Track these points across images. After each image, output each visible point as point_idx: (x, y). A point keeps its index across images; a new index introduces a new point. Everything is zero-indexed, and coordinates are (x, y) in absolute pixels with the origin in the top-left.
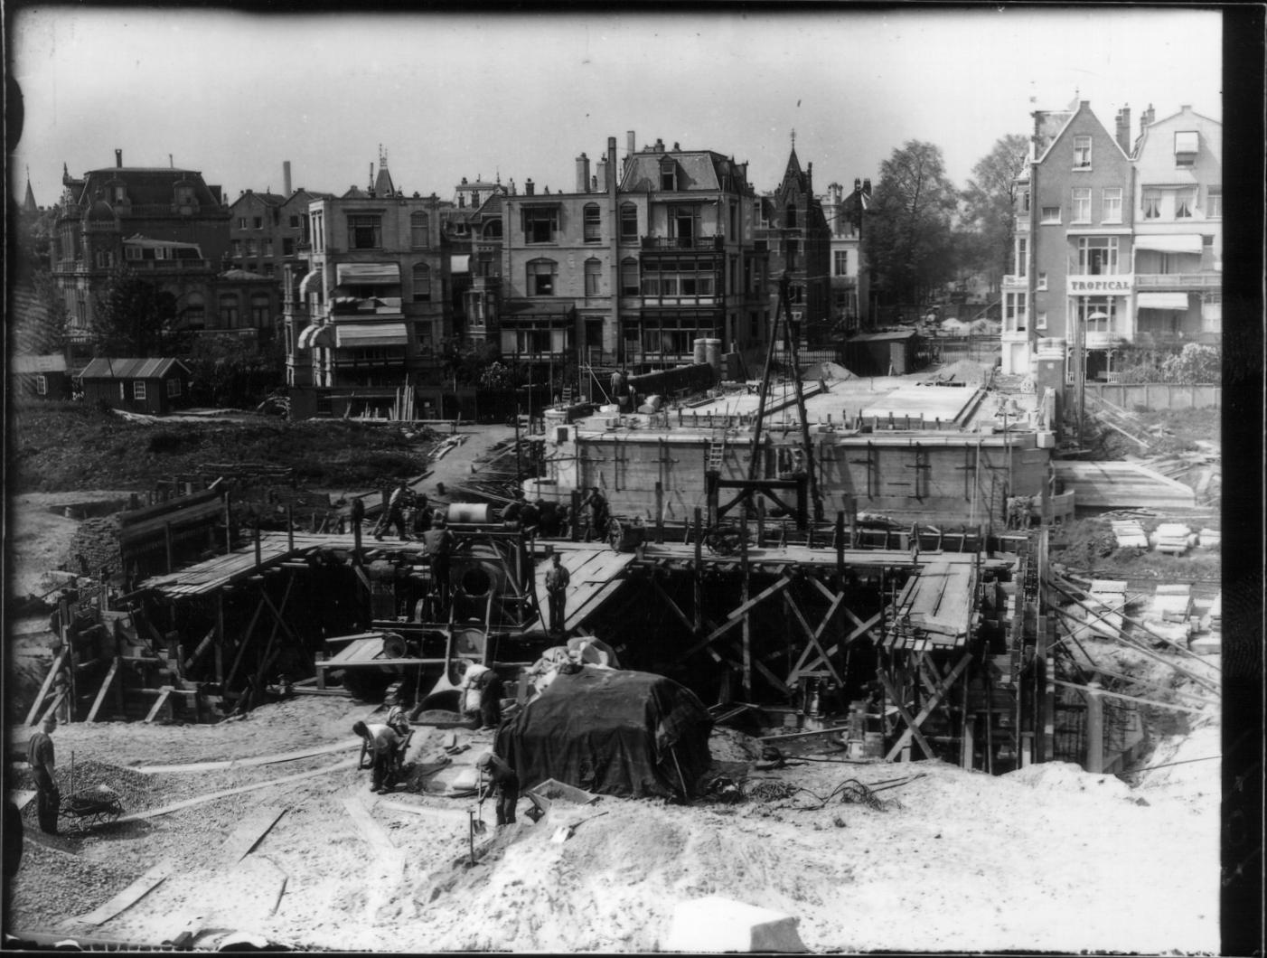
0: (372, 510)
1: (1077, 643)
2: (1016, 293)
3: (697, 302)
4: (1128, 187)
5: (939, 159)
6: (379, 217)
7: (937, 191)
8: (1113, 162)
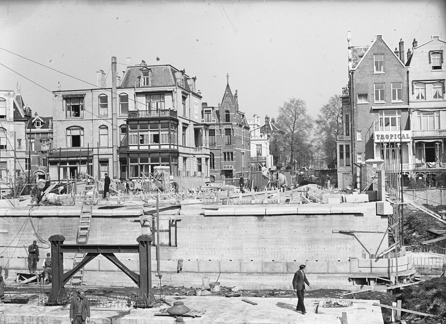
0: (80, 242)
2: (344, 144)
5: (304, 105)
7: (303, 120)
8: (396, 68)
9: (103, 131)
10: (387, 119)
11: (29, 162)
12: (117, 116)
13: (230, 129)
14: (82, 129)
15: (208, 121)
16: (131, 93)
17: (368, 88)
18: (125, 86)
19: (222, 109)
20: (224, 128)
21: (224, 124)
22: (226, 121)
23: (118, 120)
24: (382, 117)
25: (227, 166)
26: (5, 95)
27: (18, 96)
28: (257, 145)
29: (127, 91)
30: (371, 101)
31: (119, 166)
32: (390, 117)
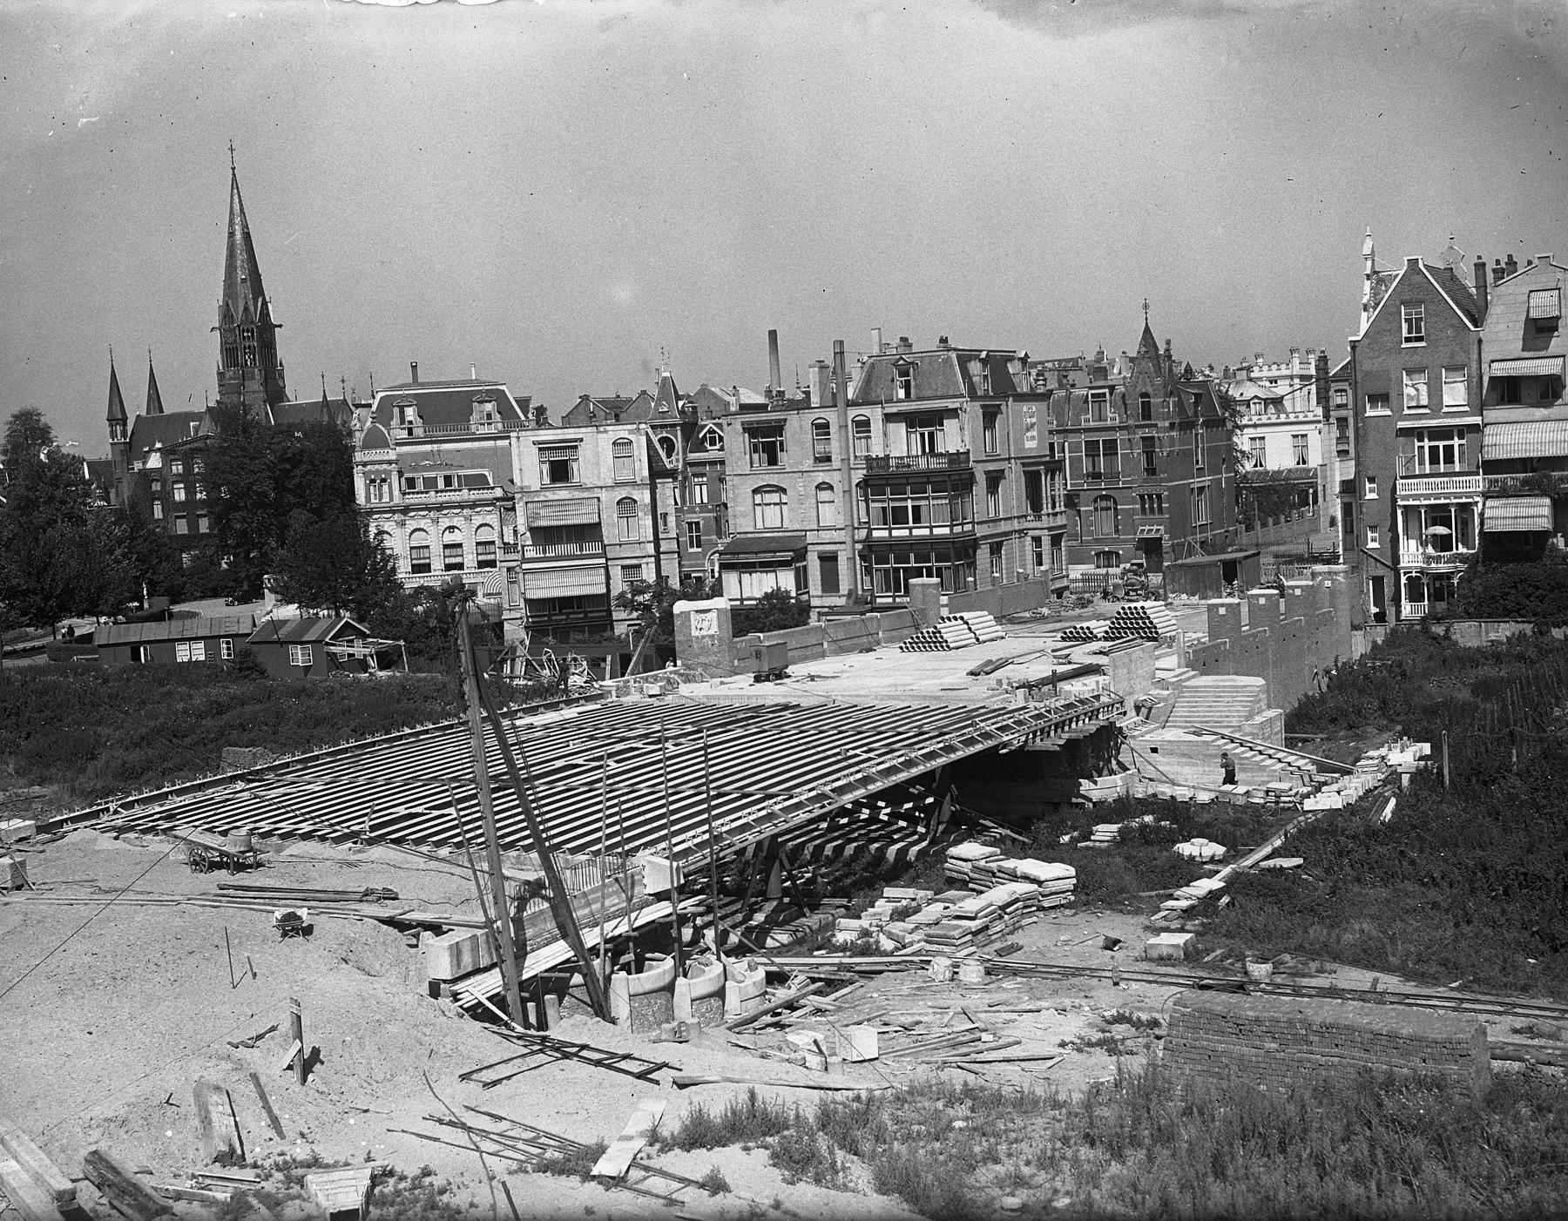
1: (821, 1052)
3: (931, 531)
4: (1474, 365)
6: (576, 447)
9: (825, 495)
10: (1434, 451)
11: (698, 530)
12: (849, 464)
13: (1153, 438)
14: (784, 491)
15: (1100, 420)
16: (875, 414)
17: (1390, 380)
18: (865, 400)
19: (1131, 390)
20: (1138, 436)
21: (1137, 427)
22: (1144, 419)
23: (852, 472)
24: (1421, 444)
25: (1147, 528)
26: (630, 432)
27: (665, 378)
28: (1294, 436)
29: (866, 411)
30: (1395, 409)
31: (858, 567)
32: (1441, 444)
